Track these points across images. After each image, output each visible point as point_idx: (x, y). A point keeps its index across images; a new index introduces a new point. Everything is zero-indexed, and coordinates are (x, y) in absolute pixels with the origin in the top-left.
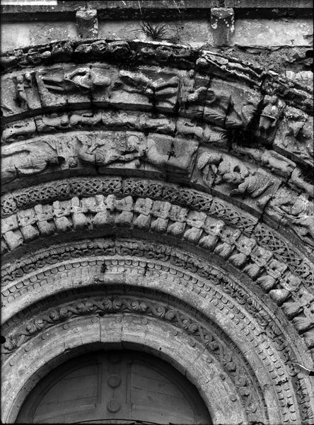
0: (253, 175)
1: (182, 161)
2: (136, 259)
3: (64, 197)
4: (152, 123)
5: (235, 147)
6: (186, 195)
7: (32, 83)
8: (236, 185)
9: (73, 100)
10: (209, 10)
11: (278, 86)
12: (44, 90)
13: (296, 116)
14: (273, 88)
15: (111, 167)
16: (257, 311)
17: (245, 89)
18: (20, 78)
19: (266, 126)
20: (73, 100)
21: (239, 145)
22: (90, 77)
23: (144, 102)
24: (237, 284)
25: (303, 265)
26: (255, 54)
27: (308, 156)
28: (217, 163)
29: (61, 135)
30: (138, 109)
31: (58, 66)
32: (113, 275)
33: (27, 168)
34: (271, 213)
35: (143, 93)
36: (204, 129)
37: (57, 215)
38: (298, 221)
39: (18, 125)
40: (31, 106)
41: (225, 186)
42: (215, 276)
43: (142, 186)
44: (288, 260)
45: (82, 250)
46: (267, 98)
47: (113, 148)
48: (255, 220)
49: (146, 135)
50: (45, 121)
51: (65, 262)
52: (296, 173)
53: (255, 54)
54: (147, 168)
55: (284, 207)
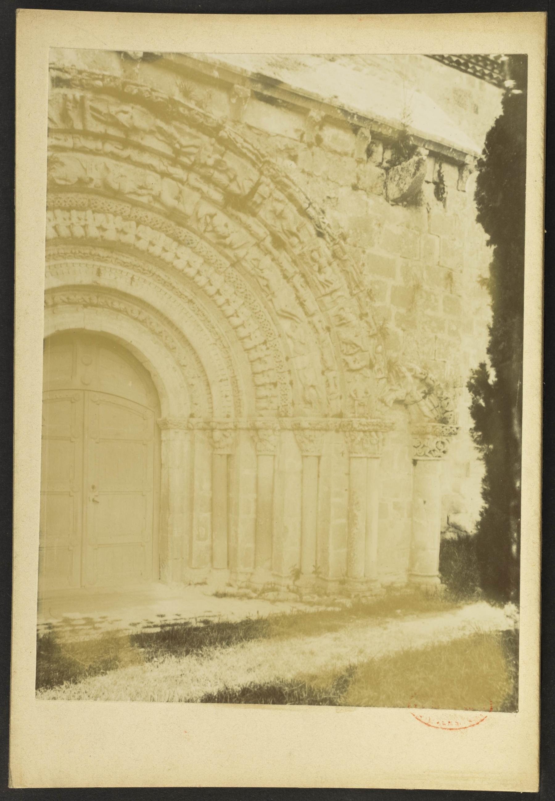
0: (237, 232)
2: (125, 270)
3: (81, 208)
4: (172, 170)
5: (230, 209)
6: (180, 233)
7: (80, 104)
9: (112, 131)
10: (232, 85)
11: (274, 172)
13: (281, 199)
14: (269, 171)
15: (127, 196)
16: (213, 328)
17: (249, 166)
18: (70, 97)
19: (259, 201)
20: (112, 131)
21: (233, 208)
23: (168, 151)
24: (201, 305)
26: (258, 134)
27: (281, 231)
28: (212, 216)
29: (92, 157)
30: (162, 155)
31: (105, 97)
32: (105, 280)
33: (60, 179)
35: (170, 145)
36: (209, 187)
37: (75, 224)
38: (262, 275)
39: (58, 137)
42: (186, 297)
43: (147, 217)
44: (246, 298)
45: (84, 254)
46: (263, 178)
47: (132, 181)
50: (82, 142)
52: (269, 239)
53: (258, 134)
55: (253, 261)
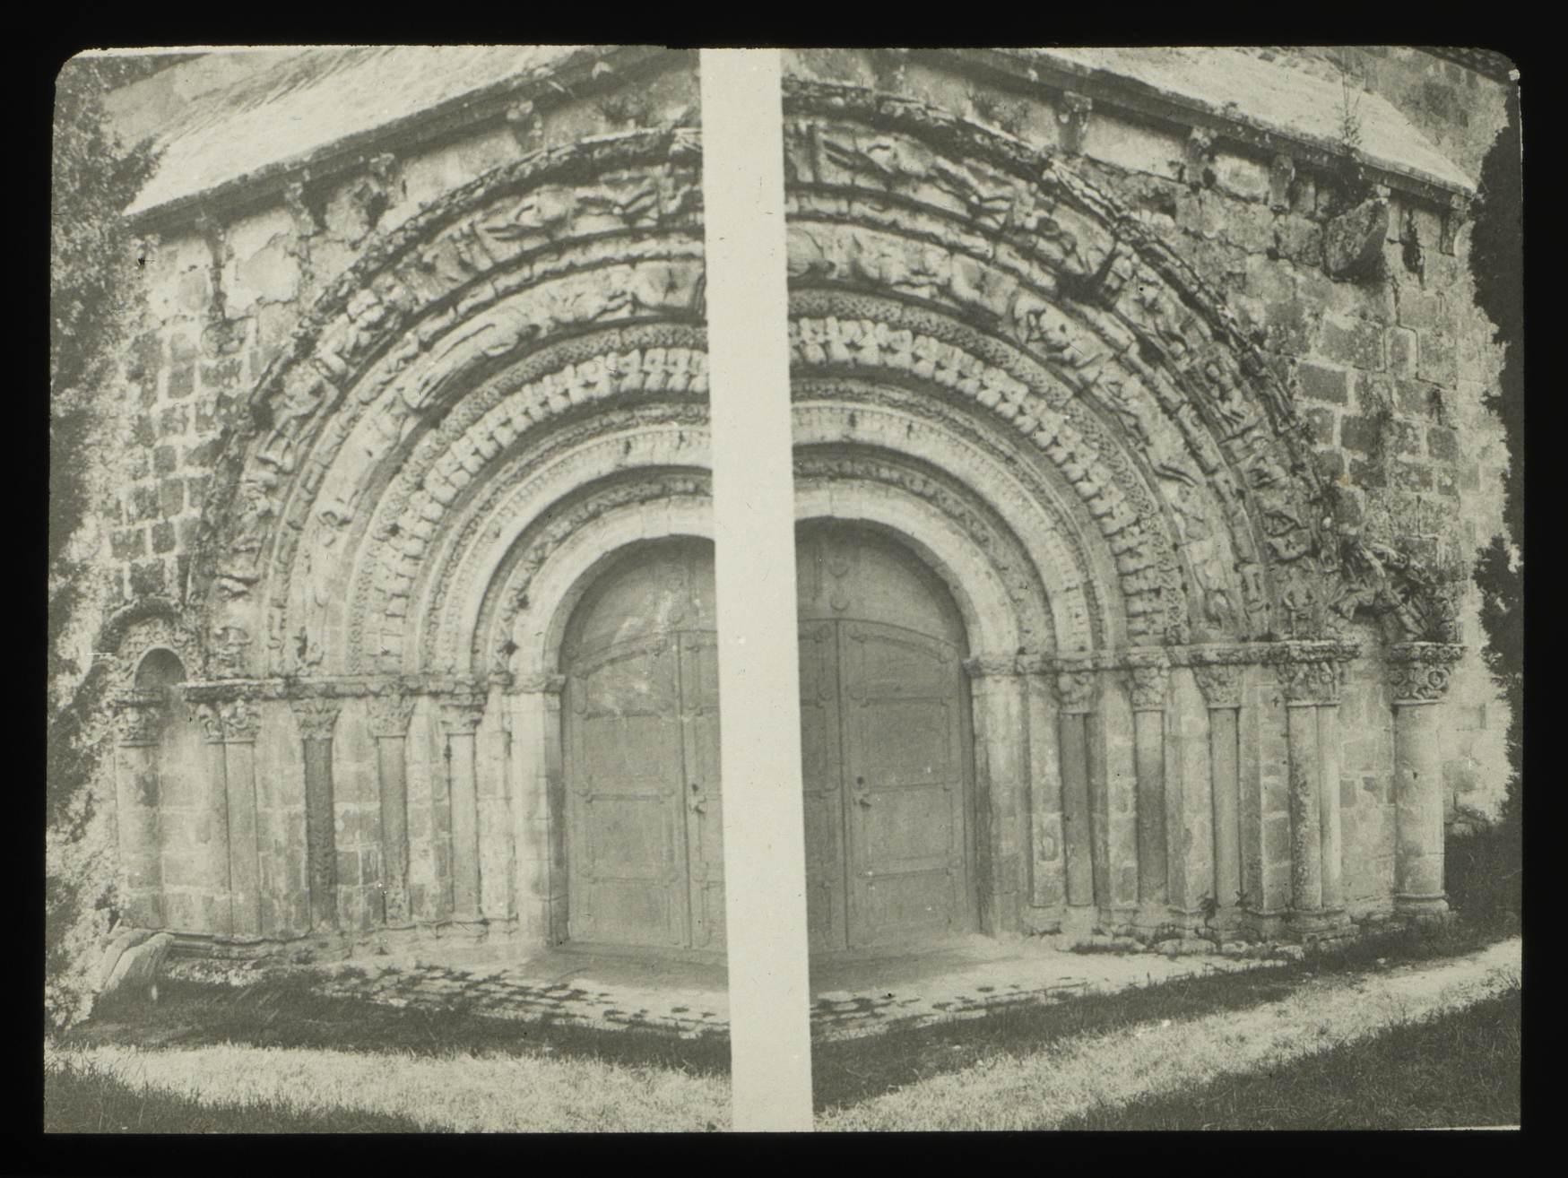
1: (998, 305)
3: (555, 369)
8: (1061, 349)
9: (863, 182)
12: (489, 240)
17: (1096, 227)
19: (1115, 285)
20: (863, 182)
22: (895, 156)
23: (961, 211)
25: (1119, 457)
29: (831, 226)
32: (867, 431)
34: (1095, 391)
35: (963, 198)
40: (800, 177)
41: (1041, 345)
48: (1069, 393)
49: (952, 254)
50: (505, 281)
51: (577, 448)
54: (945, 301)
